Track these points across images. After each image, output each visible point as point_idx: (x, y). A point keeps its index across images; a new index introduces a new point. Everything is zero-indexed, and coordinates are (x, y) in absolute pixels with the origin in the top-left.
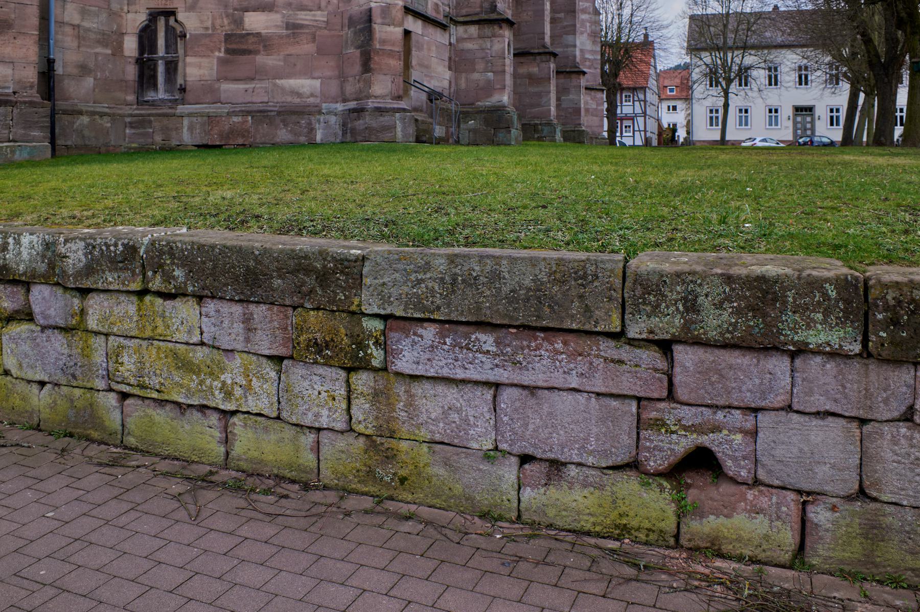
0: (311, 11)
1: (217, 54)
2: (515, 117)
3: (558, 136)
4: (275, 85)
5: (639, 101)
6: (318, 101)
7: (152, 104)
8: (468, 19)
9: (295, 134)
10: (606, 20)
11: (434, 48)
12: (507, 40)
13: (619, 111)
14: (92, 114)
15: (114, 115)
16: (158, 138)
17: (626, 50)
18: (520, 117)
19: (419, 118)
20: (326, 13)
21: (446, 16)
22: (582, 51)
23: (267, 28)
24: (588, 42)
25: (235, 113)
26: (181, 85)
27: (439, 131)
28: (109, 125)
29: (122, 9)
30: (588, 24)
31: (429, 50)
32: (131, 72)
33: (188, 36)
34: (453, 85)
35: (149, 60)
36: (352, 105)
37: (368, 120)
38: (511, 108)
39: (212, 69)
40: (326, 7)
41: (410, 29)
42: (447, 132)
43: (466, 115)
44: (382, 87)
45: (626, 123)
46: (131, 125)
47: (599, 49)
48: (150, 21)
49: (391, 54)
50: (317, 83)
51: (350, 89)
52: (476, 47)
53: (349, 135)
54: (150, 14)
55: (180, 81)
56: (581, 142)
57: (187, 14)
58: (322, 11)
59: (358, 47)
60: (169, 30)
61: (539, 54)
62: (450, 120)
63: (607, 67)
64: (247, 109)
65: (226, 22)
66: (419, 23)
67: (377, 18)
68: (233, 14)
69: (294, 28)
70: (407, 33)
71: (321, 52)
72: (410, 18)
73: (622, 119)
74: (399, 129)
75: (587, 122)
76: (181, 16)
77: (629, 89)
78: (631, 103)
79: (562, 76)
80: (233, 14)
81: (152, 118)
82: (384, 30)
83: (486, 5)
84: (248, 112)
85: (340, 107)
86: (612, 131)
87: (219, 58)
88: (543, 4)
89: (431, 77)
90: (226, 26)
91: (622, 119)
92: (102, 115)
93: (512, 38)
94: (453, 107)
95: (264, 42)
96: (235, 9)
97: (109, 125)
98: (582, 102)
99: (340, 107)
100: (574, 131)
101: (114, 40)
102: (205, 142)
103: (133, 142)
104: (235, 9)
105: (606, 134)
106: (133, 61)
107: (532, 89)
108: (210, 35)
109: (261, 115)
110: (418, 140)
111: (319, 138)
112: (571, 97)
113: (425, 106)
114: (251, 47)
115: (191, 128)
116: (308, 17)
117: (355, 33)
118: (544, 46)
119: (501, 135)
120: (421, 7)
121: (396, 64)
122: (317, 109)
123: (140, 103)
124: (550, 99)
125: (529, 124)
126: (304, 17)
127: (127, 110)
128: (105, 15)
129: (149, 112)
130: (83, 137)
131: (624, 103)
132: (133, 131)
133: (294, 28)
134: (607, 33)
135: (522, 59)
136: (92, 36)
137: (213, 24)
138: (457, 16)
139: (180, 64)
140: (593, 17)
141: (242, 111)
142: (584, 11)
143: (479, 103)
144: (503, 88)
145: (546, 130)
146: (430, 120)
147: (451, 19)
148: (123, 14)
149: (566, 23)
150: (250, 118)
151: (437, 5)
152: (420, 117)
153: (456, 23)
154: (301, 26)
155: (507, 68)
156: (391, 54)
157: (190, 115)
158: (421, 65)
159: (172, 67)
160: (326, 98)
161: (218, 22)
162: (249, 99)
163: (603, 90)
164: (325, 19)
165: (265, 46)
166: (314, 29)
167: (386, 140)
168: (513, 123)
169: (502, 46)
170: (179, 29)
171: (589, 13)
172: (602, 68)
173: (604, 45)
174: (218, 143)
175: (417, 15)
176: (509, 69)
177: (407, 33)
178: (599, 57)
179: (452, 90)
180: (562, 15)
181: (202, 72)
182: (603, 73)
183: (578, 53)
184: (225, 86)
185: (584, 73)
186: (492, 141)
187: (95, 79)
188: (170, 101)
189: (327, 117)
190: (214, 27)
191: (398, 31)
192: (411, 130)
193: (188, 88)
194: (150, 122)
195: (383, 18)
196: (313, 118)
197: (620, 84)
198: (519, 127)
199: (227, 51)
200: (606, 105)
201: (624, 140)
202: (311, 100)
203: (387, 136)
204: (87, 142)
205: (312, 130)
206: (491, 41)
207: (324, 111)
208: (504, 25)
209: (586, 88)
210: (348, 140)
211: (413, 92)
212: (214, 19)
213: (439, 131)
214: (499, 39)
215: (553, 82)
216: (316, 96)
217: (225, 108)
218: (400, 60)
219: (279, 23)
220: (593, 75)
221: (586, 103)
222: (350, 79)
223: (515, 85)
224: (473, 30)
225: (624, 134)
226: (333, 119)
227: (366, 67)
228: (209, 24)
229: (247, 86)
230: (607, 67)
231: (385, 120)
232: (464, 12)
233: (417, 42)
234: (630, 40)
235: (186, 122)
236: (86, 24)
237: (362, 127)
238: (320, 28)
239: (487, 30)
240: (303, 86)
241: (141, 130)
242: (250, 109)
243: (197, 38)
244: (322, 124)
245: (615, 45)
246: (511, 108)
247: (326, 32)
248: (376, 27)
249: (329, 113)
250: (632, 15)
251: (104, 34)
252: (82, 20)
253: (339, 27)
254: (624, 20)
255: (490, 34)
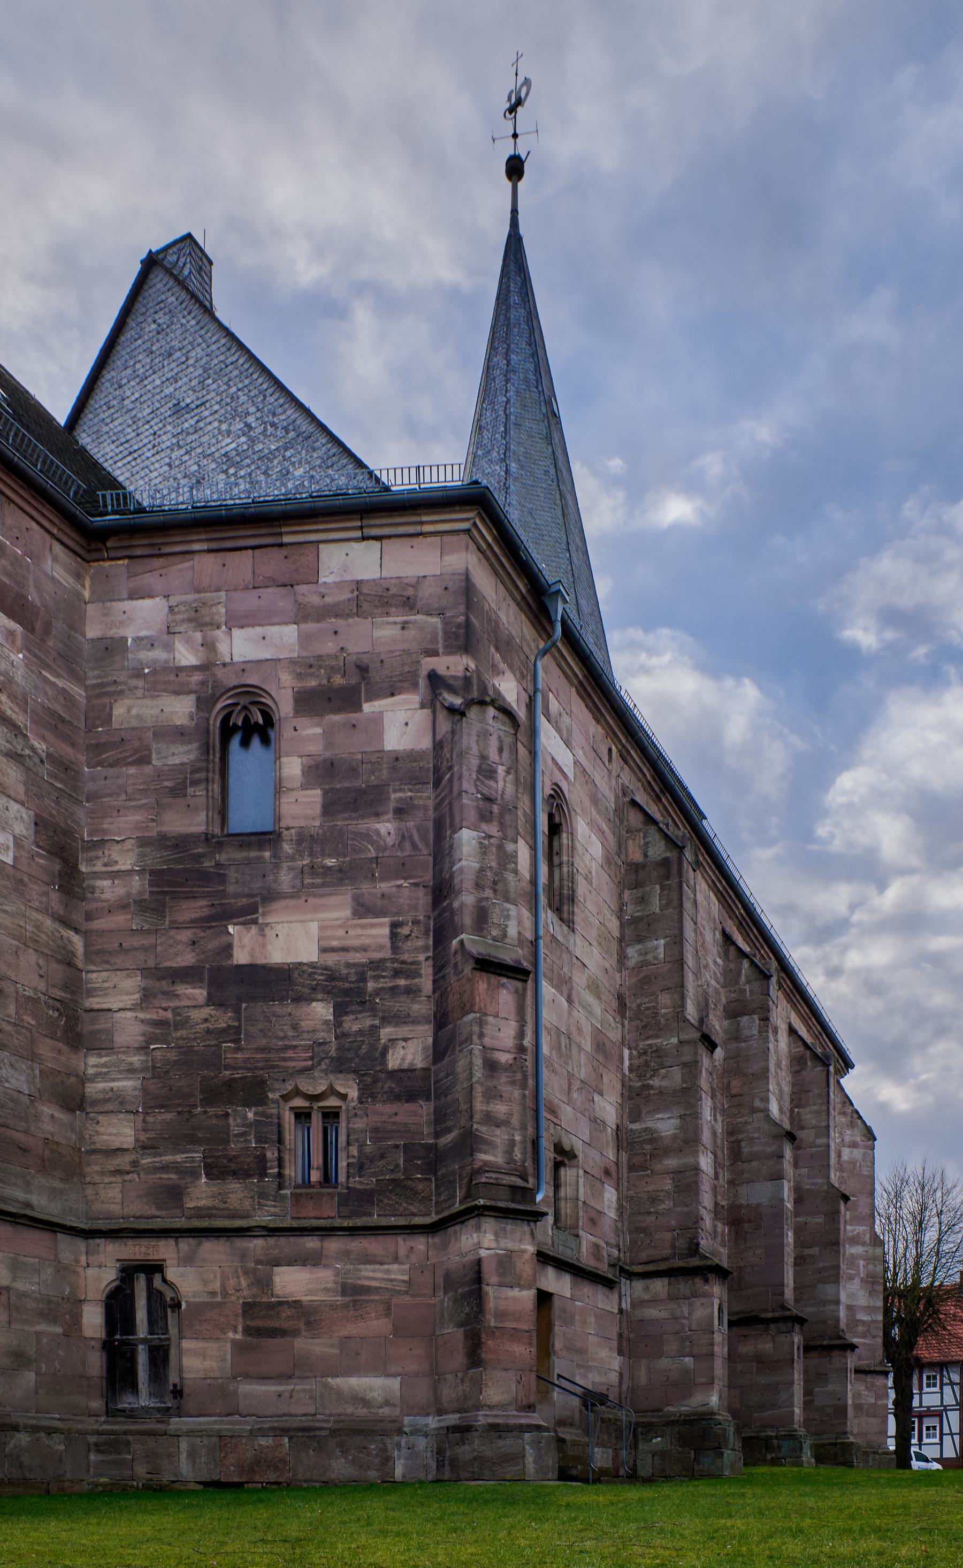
0: (382, 1264)
1: (231, 1335)
2: (731, 1430)
3: (807, 1455)
4: (326, 1386)
5: (952, 1384)
6: (397, 1412)
7: (131, 1414)
8: (651, 1268)
9: (361, 1466)
10: (895, 1251)
11: (592, 1320)
12: (716, 1302)
13: (916, 1403)
14: (35, 1429)
15: (69, 1431)
16: (141, 1470)
17: (929, 1303)
18: (738, 1430)
19: (567, 1437)
20: (407, 1267)
21: (612, 1266)
22: (849, 1308)
23: (311, 1292)
24: (861, 1293)
25: (262, 1432)
26: (175, 1386)
27: (601, 1457)
28: (62, 1447)
29: (77, 1261)
30: (862, 1263)
31: (584, 1322)
32: (96, 1363)
33: (183, 1307)
34: (626, 1378)
35: (123, 1343)
36: (452, 1419)
37: (474, 1447)
38: (724, 1416)
39: (223, 1360)
40: (408, 1257)
41: (550, 1290)
42: (616, 1458)
43: (648, 1429)
44: (499, 1391)
45: (927, 1422)
46: (98, 1448)
47: (880, 1303)
48: (122, 1280)
49: (515, 1335)
50: (394, 1384)
51: (448, 1393)
52: (664, 1314)
53: (447, 1468)
54: (123, 1270)
55: (173, 1378)
56: (849, 1464)
57: (181, 1269)
58: (401, 1263)
59: (460, 1325)
60: (154, 1296)
61: (775, 1320)
62: (619, 1438)
63: (896, 1331)
64: (282, 1425)
65: (244, 1283)
66: (567, 1279)
67: (491, 1276)
68: (255, 1271)
69: (354, 1293)
70: (544, 1298)
71: (399, 1331)
72: (551, 1272)
73: (921, 1417)
74: (530, 1459)
75: (857, 1428)
76: (172, 1273)
77: (931, 1365)
78: (937, 1389)
79: (814, 1354)
80: (255, 1271)
81: (130, 1438)
82: (503, 1295)
83: (682, 1243)
84: (282, 1430)
85: (433, 1422)
86: (903, 1438)
87: (234, 1342)
88: (782, 1235)
89: (589, 1369)
90: (243, 1288)
91: (921, 1417)
92: (50, 1431)
93: (725, 1298)
94: (622, 1415)
95: (306, 1315)
96: (259, 1262)
97: (62, 1447)
98: (850, 1395)
99: (433, 1422)
100: (835, 1444)
101: (65, 1309)
102: (215, 1477)
103: (102, 1476)
104: (259, 1262)
105: (892, 1446)
106: (98, 1345)
107: (762, 1380)
108: (219, 1305)
109: (304, 1434)
110: (564, 1475)
111: (399, 1472)
112: (830, 1387)
113: (577, 1416)
114: (285, 1325)
115: (193, 1455)
116: (379, 1275)
117: (455, 1301)
118: (783, 1307)
119: (707, 1461)
120: (569, 1252)
121: (524, 1351)
122: (396, 1425)
123: (111, 1412)
124: (793, 1395)
125: (757, 1438)
126: (371, 1274)
127: (91, 1424)
128: (50, 1271)
129: (126, 1427)
130: (21, 1466)
131: (926, 1390)
132: (101, 1457)
133: (354, 1293)
134: (895, 1274)
135: (745, 1331)
136: (31, 1305)
137: (223, 1286)
138: (632, 1263)
139: (173, 1352)
140: (871, 1250)
141: (274, 1429)
142: (855, 1241)
143: (670, 1408)
144: (711, 1382)
145: (786, 1445)
146: (586, 1439)
147: (622, 1270)
148: (80, 1270)
149: (821, 1265)
150: (286, 1440)
151: (596, 1246)
152: (567, 1434)
153: (631, 1275)
154: (367, 1290)
155: (717, 1349)
156: (515, 1335)
157: (190, 1433)
158: (570, 1349)
159: (160, 1356)
160: (410, 1407)
161: (232, 1282)
162: (284, 1409)
163: (886, 1374)
164: (406, 1278)
165: (308, 1323)
166: (387, 1295)
167: (508, 1477)
168: (726, 1440)
169: (709, 1311)
170: (169, 1295)
171: (864, 1244)
172: (887, 1334)
173: (889, 1294)
174: (236, 1480)
175: (562, 1265)
176: (720, 1350)
177: (544, 1298)
178: (880, 1318)
179: (624, 1387)
180: (815, 1250)
181: (208, 1364)
182: (888, 1341)
183: (842, 1313)
184: (246, 1388)
185: (853, 1347)
186: (691, 1474)
187: (38, 1374)
188: (159, 1410)
189: (411, 1438)
190: (225, 1293)
191: (527, 1297)
192: (551, 1461)
193: (186, 1391)
194: (128, 1443)
195: (501, 1275)
196: (388, 1441)
197: (917, 1359)
198: (738, 1445)
199: (248, 1331)
200: (892, 1395)
201: (925, 1451)
202: (385, 1411)
203: (511, 1470)
204: (28, 1475)
205: (387, 1460)
206: (690, 1305)
207: (406, 1429)
208: (711, 1277)
209: (858, 1371)
210: (446, 1477)
211: (556, 1394)
212: (224, 1278)
213: (601, 1457)
214: (703, 1300)
215: (798, 1366)
216: (394, 1405)
217: (247, 1423)
218: (530, 1344)
219: (330, 1285)
220: (868, 1346)
221: (857, 1395)
222: (449, 1377)
223: (732, 1374)
224: (659, 1286)
225: (925, 1441)
226: (421, 1443)
227: (475, 1357)
228: (217, 1286)
229: (280, 1388)
230: (896, 1331)
231: (506, 1444)
232: (644, 1256)
233: (564, 1311)
234: (937, 1283)
235: (184, 1445)
236: (20, 1286)
237: (468, 1457)
238: (398, 1292)
239: (683, 1286)
240: (371, 1389)
241: (114, 1457)
242: (287, 1425)
243: (198, 1309)
244: (404, 1451)
245: (911, 1293)
246: (724, 1416)
247: (408, 1298)
248: (490, 1291)
249: (416, 1432)
250: (939, 1240)
251: (49, 1302)
252: (14, 1279)
253: (429, 1291)
254: (926, 1250)
255: (688, 1293)
